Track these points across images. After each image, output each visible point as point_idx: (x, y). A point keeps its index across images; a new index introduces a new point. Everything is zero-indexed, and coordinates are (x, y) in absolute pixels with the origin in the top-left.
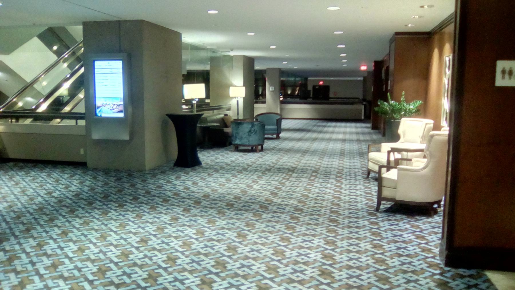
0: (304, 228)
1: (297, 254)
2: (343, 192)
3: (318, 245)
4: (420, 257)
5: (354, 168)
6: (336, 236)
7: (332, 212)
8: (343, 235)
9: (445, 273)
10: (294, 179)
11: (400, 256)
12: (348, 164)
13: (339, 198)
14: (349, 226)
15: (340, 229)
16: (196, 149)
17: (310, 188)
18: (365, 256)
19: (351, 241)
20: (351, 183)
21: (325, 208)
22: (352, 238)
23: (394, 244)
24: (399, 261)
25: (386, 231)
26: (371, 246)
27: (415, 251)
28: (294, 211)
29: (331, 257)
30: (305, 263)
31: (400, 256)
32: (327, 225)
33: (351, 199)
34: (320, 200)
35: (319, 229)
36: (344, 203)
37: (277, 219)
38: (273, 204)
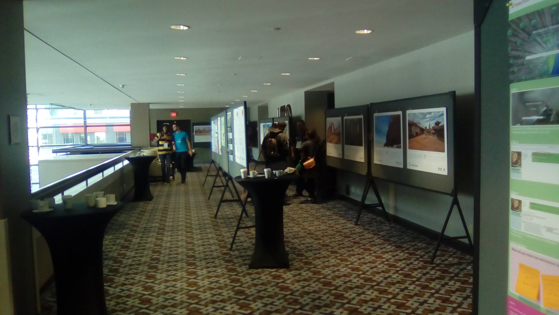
0: (164, 275)
1: (164, 300)
2: (195, 237)
3: (181, 277)
4: (280, 296)
5: (203, 223)
6: (197, 289)
7: (189, 257)
8: (203, 275)
9: (304, 307)
10: (140, 235)
11: (256, 285)
12: (196, 215)
13: (192, 243)
14: (207, 266)
15: (201, 293)
16: (223, 116)
17: (160, 243)
18: (229, 304)
19: (213, 292)
20: (202, 232)
21: (181, 255)
22: (210, 267)
23: (260, 300)
24: (256, 290)
25: (249, 287)
26: (238, 307)
27: (274, 291)
28: (148, 269)
29: (195, 284)
30: (173, 292)
31: (256, 285)
32: (187, 279)
33: (204, 242)
34: (174, 254)
35: (179, 274)
36: (199, 254)
37: (135, 271)
38: (127, 257)
